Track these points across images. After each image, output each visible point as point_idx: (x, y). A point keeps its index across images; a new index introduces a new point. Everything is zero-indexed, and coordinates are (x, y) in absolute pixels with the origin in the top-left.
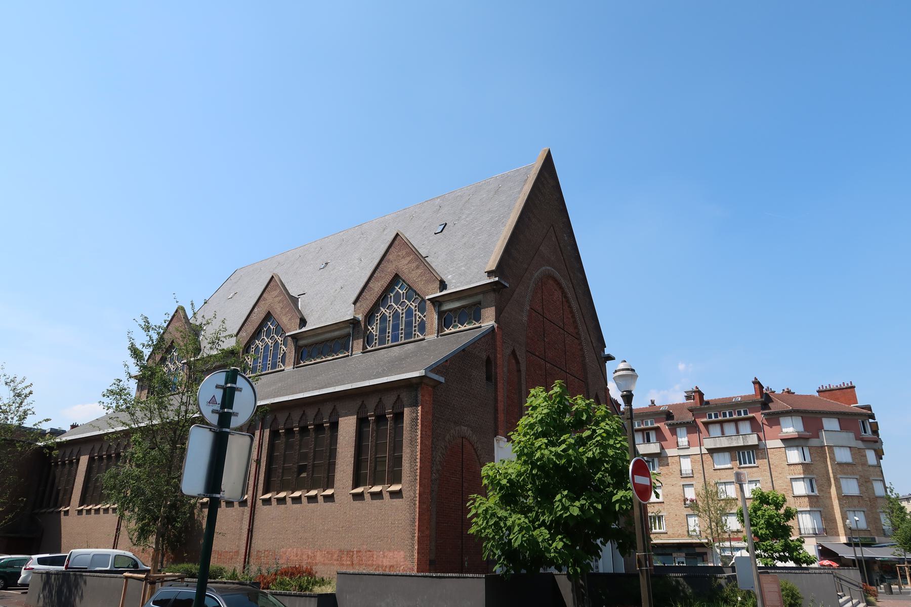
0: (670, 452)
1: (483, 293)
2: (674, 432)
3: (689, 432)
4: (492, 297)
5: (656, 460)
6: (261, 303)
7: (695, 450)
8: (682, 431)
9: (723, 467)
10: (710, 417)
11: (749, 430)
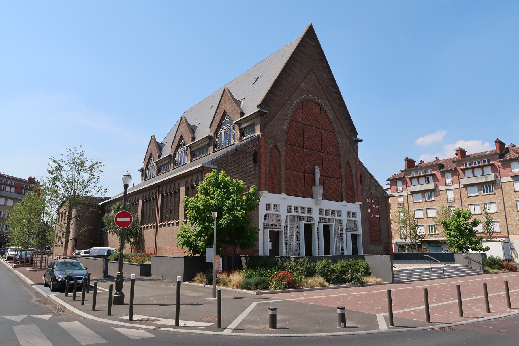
0: (441, 188)
1: (256, 117)
2: (443, 176)
3: (452, 176)
4: (259, 119)
5: (433, 193)
6: (179, 130)
7: (456, 186)
8: (448, 175)
9: (473, 195)
10: (466, 165)
11: (490, 172)
